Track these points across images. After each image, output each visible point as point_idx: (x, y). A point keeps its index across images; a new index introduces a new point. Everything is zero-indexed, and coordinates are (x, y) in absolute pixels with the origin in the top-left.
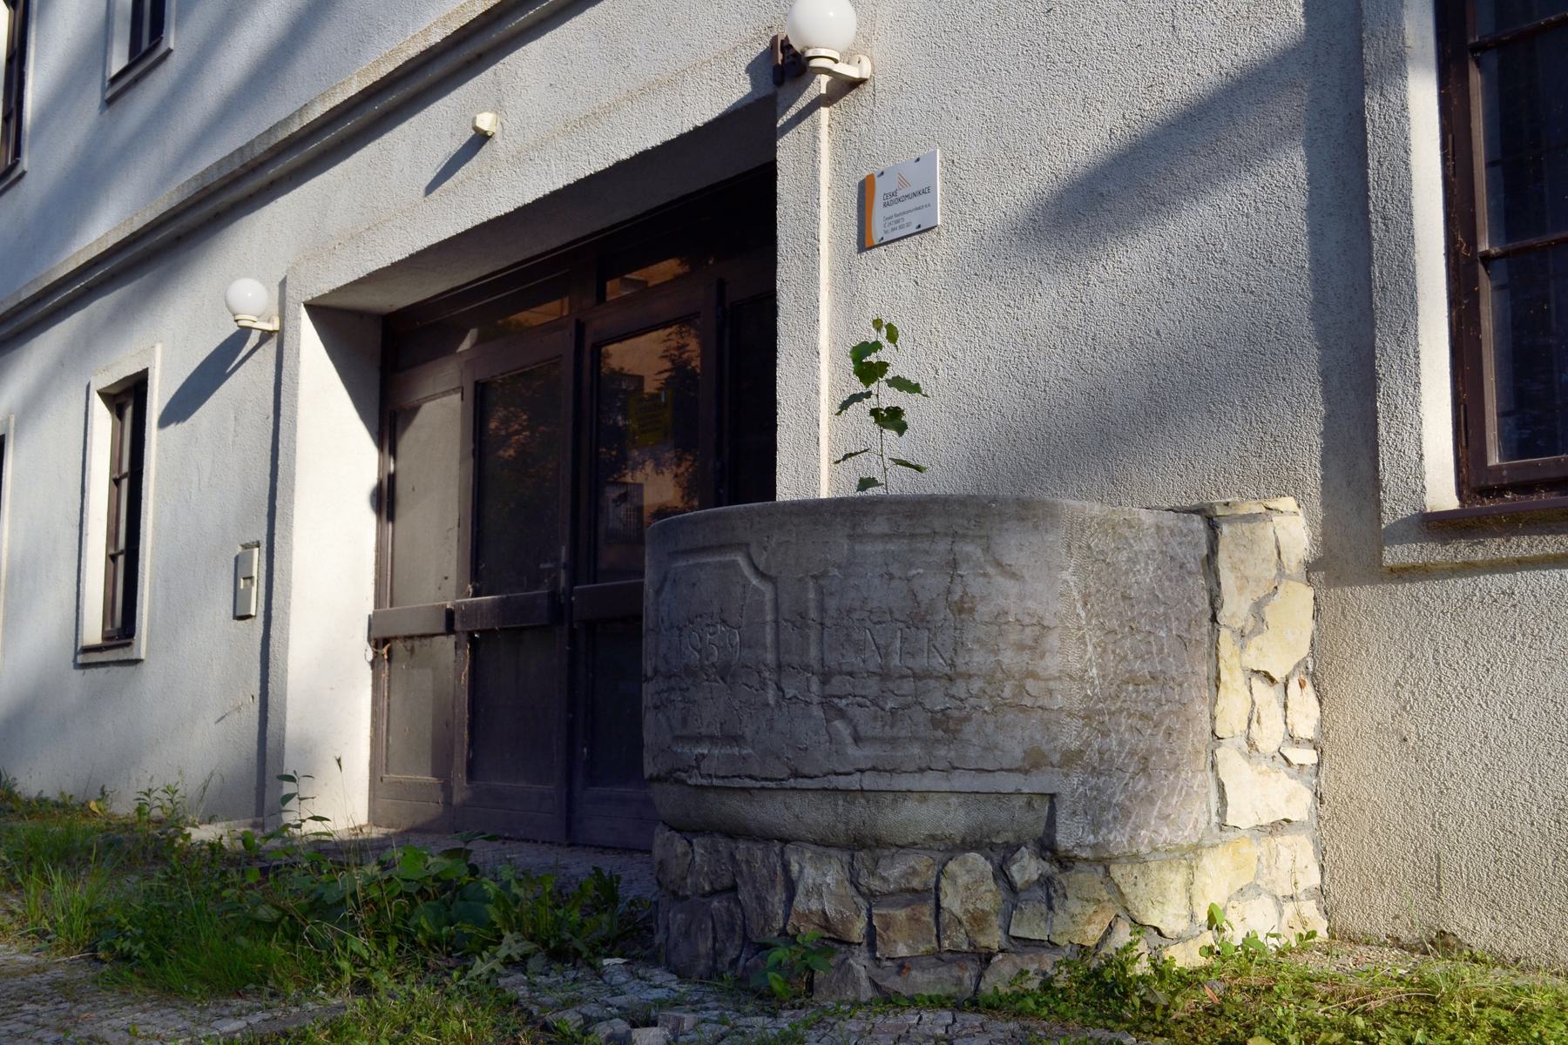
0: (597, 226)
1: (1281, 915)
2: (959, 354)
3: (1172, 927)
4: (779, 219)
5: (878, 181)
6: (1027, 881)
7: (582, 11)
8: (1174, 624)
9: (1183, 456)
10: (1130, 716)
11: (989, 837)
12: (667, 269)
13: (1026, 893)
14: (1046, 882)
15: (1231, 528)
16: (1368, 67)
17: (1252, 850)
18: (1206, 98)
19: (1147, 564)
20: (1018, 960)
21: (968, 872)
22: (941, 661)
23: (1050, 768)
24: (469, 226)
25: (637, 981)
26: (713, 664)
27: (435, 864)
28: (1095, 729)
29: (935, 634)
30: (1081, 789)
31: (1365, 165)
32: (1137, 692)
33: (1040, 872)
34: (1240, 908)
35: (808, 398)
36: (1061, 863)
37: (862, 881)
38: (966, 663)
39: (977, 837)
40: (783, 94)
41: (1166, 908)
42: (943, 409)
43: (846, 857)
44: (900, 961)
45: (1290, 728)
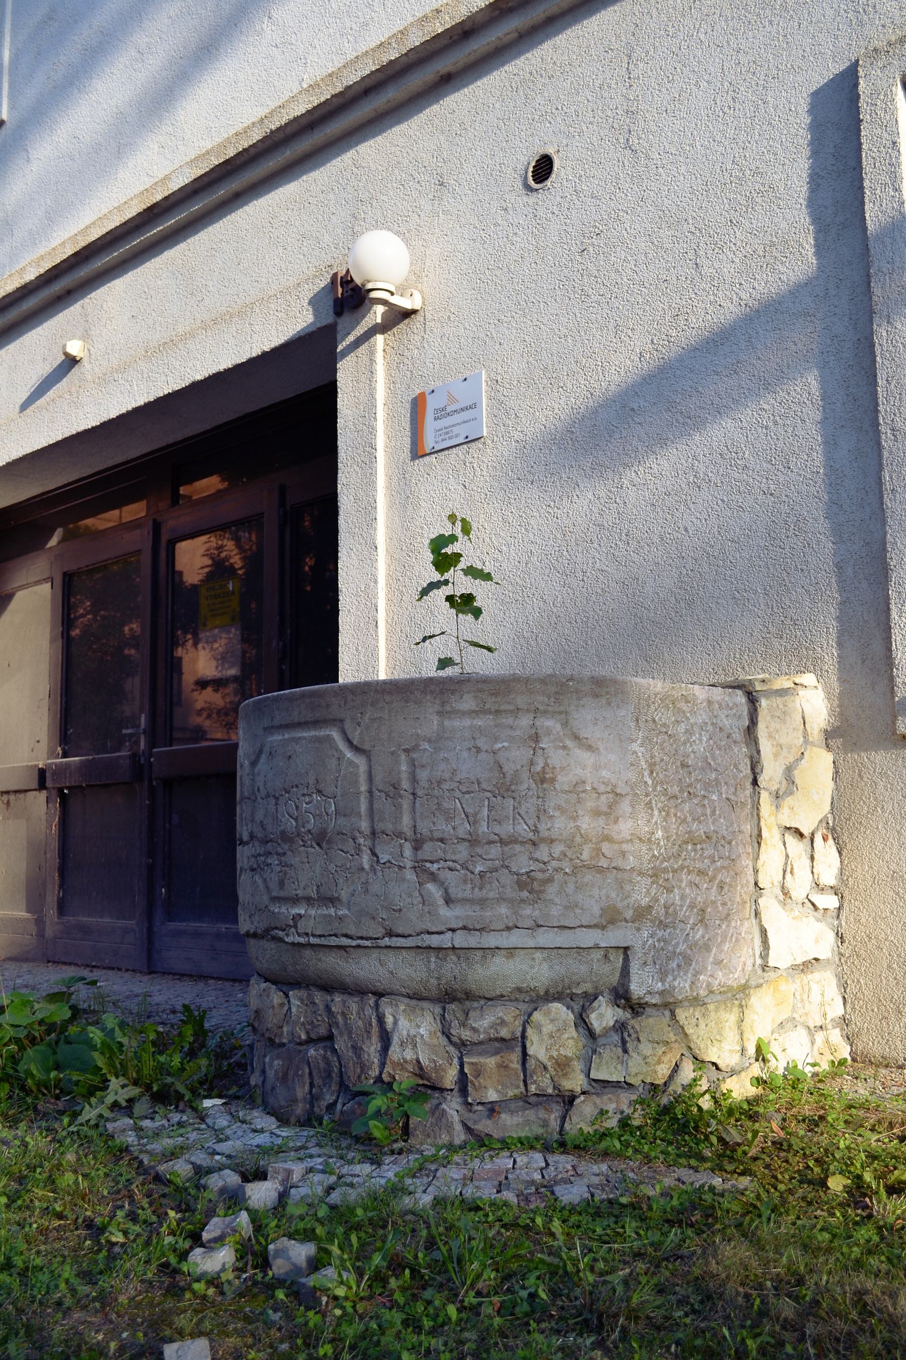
0: (171, 439)
1: (813, 1043)
2: (504, 548)
3: (727, 1061)
4: (339, 431)
5: (429, 399)
6: (604, 1028)
7: (162, 252)
8: (724, 789)
9: (710, 637)
10: (689, 872)
11: (570, 988)
12: (210, 484)
13: (603, 1039)
14: (620, 1027)
15: (769, 702)
16: (875, 298)
17: (789, 987)
18: (727, 326)
19: (701, 735)
20: (598, 1101)
21: (552, 1021)
22: (526, 827)
23: (624, 923)
24: (60, 438)
25: (239, 1124)
26: (309, 831)
27: (40, 1009)
28: (661, 886)
29: (520, 803)
30: (650, 941)
31: (875, 384)
32: (695, 850)
33: (615, 1018)
34: (781, 1039)
35: (367, 586)
36: (633, 1009)
37: (453, 1031)
38: (549, 829)
39: (560, 989)
40: (343, 322)
41: (723, 1045)
42: (490, 596)
43: (438, 1010)
44: (490, 1106)
45: (816, 877)
